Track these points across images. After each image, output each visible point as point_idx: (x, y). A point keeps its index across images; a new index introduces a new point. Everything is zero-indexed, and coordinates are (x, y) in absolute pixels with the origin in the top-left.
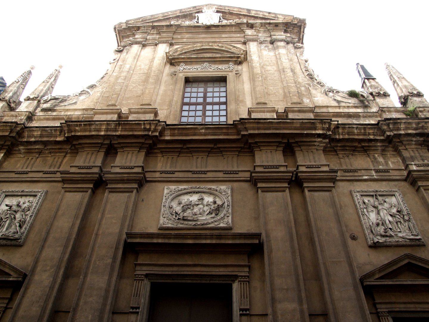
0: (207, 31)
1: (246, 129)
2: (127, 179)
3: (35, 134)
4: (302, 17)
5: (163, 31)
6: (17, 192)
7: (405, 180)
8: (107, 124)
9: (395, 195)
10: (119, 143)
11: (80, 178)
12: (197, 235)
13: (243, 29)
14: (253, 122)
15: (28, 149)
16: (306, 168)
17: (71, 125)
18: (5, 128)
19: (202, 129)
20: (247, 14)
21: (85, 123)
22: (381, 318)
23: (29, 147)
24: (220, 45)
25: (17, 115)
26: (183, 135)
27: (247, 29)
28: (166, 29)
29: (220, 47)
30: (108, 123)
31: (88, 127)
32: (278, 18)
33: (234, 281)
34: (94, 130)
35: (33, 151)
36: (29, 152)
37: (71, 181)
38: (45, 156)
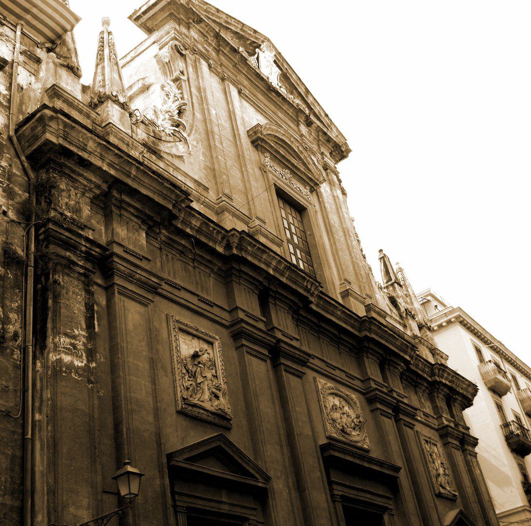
0: (266, 92)
1: (370, 330)
3: (192, 222)
4: (351, 147)
5: (224, 50)
6: (191, 327)
7: (437, 430)
8: (280, 261)
9: (214, 345)
10: (276, 292)
11: (260, 338)
12: (373, 460)
13: (300, 121)
15: (170, 239)
16: (124, 251)
18: (169, 194)
19: (340, 310)
20: (303, 94)
21: (260, 247)
22: (178, 514)
23: (174, 237)
24: (300, 148)
25: (130, 143)
26: (324, 310)
27: (303, 124)
29: (299, 150)
30: (281, 260)
31: (259, 253)
32: (332, 129)
33: (384, 513)
34: (264, 262)
35: (175, 246)
36: (169, 244)
37: (153, 288)
38: (185, 260)
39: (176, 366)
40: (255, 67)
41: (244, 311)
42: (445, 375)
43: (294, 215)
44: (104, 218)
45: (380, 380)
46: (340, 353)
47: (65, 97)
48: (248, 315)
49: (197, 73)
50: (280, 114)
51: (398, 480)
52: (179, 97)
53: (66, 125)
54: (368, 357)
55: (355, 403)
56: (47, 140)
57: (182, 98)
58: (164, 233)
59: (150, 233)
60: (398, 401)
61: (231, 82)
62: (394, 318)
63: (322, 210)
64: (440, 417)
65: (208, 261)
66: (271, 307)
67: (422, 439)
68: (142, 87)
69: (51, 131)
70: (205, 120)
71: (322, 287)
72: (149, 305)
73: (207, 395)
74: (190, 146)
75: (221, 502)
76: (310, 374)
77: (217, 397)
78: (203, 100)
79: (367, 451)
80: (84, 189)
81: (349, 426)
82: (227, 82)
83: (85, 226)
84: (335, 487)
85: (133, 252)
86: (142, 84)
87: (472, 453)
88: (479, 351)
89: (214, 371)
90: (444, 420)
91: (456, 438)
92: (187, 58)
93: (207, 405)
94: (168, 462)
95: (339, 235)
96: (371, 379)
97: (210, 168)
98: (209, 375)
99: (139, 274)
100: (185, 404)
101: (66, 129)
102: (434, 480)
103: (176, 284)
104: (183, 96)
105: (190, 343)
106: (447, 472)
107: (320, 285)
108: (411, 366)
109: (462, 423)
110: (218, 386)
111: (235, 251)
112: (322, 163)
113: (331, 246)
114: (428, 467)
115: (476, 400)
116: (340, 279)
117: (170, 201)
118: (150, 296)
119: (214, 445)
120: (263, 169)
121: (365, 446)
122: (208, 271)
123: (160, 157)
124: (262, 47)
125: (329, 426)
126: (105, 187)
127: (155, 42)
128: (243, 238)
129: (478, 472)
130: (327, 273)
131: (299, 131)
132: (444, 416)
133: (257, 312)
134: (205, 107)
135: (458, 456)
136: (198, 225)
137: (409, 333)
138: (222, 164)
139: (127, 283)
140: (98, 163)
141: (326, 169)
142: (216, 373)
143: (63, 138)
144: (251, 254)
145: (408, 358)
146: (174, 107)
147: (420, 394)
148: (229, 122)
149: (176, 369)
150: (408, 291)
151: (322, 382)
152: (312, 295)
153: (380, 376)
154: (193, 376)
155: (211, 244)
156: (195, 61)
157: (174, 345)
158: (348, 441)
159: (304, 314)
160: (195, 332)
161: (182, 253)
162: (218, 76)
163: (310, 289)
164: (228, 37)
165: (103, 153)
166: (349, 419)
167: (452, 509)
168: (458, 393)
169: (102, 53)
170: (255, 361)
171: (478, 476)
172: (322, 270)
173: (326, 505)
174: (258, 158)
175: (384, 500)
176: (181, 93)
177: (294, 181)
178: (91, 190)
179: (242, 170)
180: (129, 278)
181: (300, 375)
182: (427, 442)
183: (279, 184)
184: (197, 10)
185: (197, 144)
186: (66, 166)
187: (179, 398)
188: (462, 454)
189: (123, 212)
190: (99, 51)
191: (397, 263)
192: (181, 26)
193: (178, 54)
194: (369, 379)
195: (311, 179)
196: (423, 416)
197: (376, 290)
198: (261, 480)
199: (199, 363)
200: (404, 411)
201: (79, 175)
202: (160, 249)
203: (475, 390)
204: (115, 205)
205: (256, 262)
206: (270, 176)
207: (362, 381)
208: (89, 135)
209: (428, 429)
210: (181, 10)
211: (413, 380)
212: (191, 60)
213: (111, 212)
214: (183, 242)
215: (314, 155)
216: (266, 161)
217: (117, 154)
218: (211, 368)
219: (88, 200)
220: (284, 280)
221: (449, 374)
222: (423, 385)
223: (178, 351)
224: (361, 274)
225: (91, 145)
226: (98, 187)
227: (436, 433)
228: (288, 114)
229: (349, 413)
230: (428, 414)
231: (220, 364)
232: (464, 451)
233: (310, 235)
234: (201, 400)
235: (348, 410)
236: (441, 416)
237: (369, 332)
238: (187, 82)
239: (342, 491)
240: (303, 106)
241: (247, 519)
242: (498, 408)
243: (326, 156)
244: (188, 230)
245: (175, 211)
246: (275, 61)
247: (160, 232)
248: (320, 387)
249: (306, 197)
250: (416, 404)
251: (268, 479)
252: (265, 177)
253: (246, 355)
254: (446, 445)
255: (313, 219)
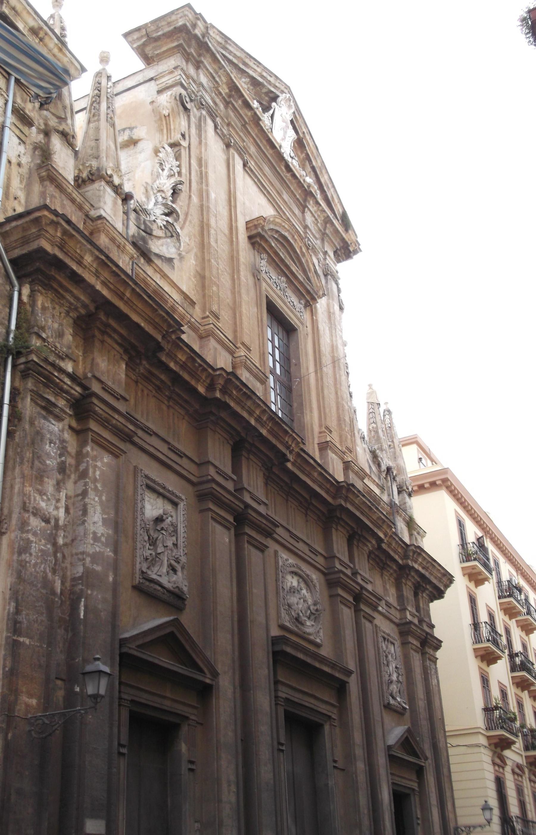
1: (346, 499)
2: (106, 418)
6: (159, 484)
7: (397, 625)
9: (179, 506)
14: (152, 306)
15: (150, 372)
17: (234, 382)
21: (247, 391)
23: (156, 372)
26: (299, 469)
28: (239, 106)
34: (247, 410)
39: (138, 532)
40: (267, 129)
41: (216, 467)
42: (420, 560)
43: (281, 337)
44: (83, 341)
45: (346, 560)
46: (307, 521)
47: (59, 181)
48: (219, 472)
49: (200, 136)
50: (286, 196)
51: (347, 685)
52: (176, 171)
53: (65, 232)
54: (337, 530)
55: (315, 586)
56: (41, 247)
57: (179, 173)
58: (144, 365)
59: (131, 365)
60: (362, 588)
61: (237, 151)
62: (372, 478)
63: (313, 333)
64: (403, 610)
65: (186, 401)
66: (243, 462)
67: (379, 635)
68: (127, 141)
69: (46, 237)
70: (202, 206)
71: (304, 444)
72: (121, 457)
73: (165, 569)
74: (182, 244)
75: (165, 697)
76: (273, 546)
77: (174, 570)
78: (203, 177)
79: (318, 646)
80: (70, 307)
81: (304, 614)
82: (232, 151)
83: (67, 356)
84: (280, 687)
85: (112, 389)
86: (129, 135)
87: (432, 658)
88: (461, 525)
89: (174, 538)
90: (408, 613)
91: (417, 638)
92: (191, 114)
93: (164, 581)
94: (121, 646)
95: (328, 370)
96: (337, 557)
97: (200, 274)
98: (170, 544)
99: (116, 419)
100: (144, 578)
101: (64, 237)
102: (385, 687)
103: (149, 428)
104: (181, 170)
105: (155, 502)
106: (400, 678)
107: (302, 442)
108: (384, 546)
109: (426, 619)
110: (177, 558)
111: (218, 395)
112: (323, 265)
113: (317, 380)
114: (381, 672)
115: (449, 593)
116: (320, 426)
117: (160, 331)
118: (122, 445)
119: (168, 631)
120: (256, 274)
121: (318, 640)
122: (183, 412)
123: (149, 261)
124: (279, 100)
125: (283, 613)
126: (92, 308)
127: (151, 79)
128: (230, 380)
129: (434, 682)
130: (307, 418)
131: (304, 219)
132: (409, 609)
133: (228, 470)
134: (204, 187)
135: (416, 660)
136: (184, 360)
137: (385, 498)
138: (214, 272)
139: (101, 428)
140: (91, 279)
141: (326, 275)
142: (177, 540)
143: (59, 247)
144: (235, 399)
145: (382, 535)
146: (167, 184)
147: (386, 578)
148: (227, 208)
149: (138, 535)
150: (393, 441)
151: (284, 555)
152: (291, 452)
153: (347, 553)
154: (153, 543)
155: (193, 383)
156: (200, 120)
157: (140, 505)
158: (301, 633)
159: (277, 472)
160: (161, 491)
161: (159, 389)
162: (223, 140)
163: (291, 445)
164: (243, 84)
165: (99, 269)
166: (306, 605)
167: (398, 724)
168: (430, 582)
169: (97, 106)
170: (219, 528)
171: (434, 687)
172: (302, 413)
173: (268, 709)
174: (253, 259)
175: (328, 707)
176: (179, 166)
177: (289, 292)
178: (76, 309)
179: (233, 276)
180: (104, 423)
181: (262, 548)
182: (384, 639)
183: (272, 297)
184: (213, 46)
185: (190, 240)
186: (55, 279)
187: (138, 571)
188: (421, 658)
189: (106, 338)
190: (94, 102)
191: (386, 403)
192: (190, 64)
193: (181, 108)
194: (335, 557)
195: (308, 292)
196: (385, 607)
197: (358, 441)
198: (208, 675)
199: (162, 529)
200: (367, 601)
201: (67, 290)
202: (137, 382)
203: (449, 579)
204: (99, 329)
205: (238, 409)
206: (264, 285)
207: (325, 558)
208: (89, 246)
209: (388, 622)
210: (193, 42)
211: (381, 560)
212: (195, 117)
213: (94, 336)
214: (163, 377)
215: (316, 255)
216: (262, 265)
217: (114, 272)
218: (172, 534)
219: (71, 321)
220: (264, 432)
221: (424, 559)
222: (391, 568)
223: (143, 514)
224: (345, 420)
225: (88, 259)
226: (85, 306)
227: (396, 629)
228: (295, 196)
229: (306, 597)
230: (391, 604)
231: (182, 531)
232: (424, 654)
233: (296, 365)
234: (158, 574)
235: (306, 594)
236: (405, 609)
237: (345, 501)
238: (187, 150)
239: (287, 694)
240: (315, 189)
241: (187, 718)
242: (471, 602)
243: (329, 256)
244: (172, 365)
245: (164, 344)
246: (292, 122)
247: (141, 364)
248: (281, 563)
249: (298, 314)
250: (380, 591)
251: (215, 674)
252: (258, 287)
253: (211, 521)
254: (404, 644)
255: (302, 346)
